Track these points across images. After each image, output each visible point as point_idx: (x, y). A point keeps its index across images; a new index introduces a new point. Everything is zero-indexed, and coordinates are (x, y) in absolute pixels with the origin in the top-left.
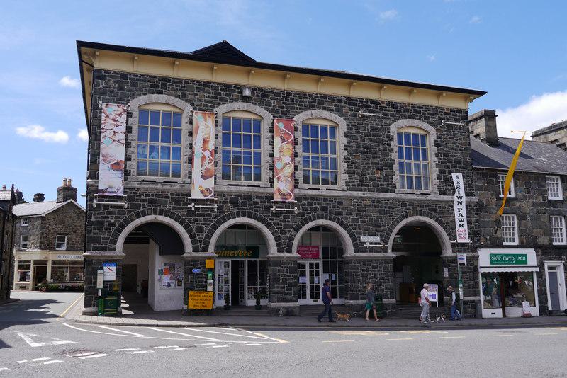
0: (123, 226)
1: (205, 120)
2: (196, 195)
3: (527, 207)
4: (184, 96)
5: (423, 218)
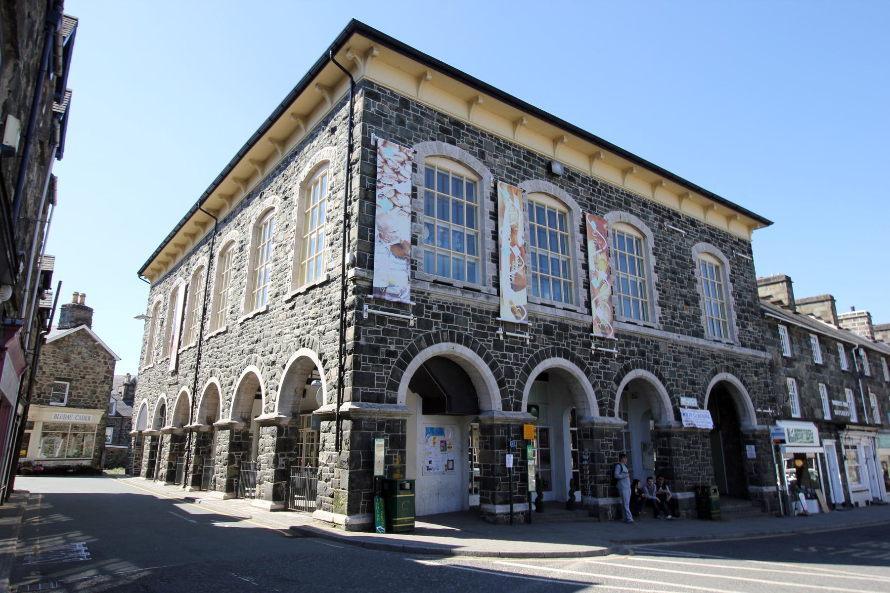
0: (408, 358)
1: (512, 198)
2: (506, 315)
5: (730, 377)
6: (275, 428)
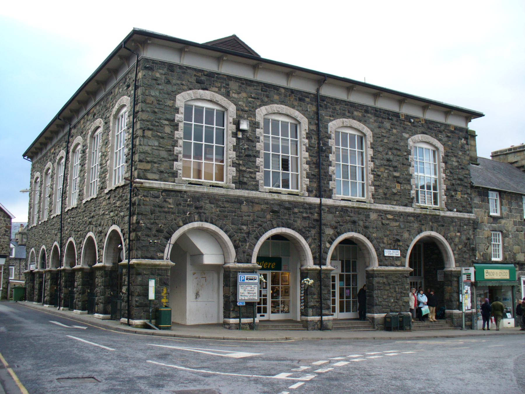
3: (508, 224)
4: (227, 95)
5: (434, 234)
6: (103, 271)
